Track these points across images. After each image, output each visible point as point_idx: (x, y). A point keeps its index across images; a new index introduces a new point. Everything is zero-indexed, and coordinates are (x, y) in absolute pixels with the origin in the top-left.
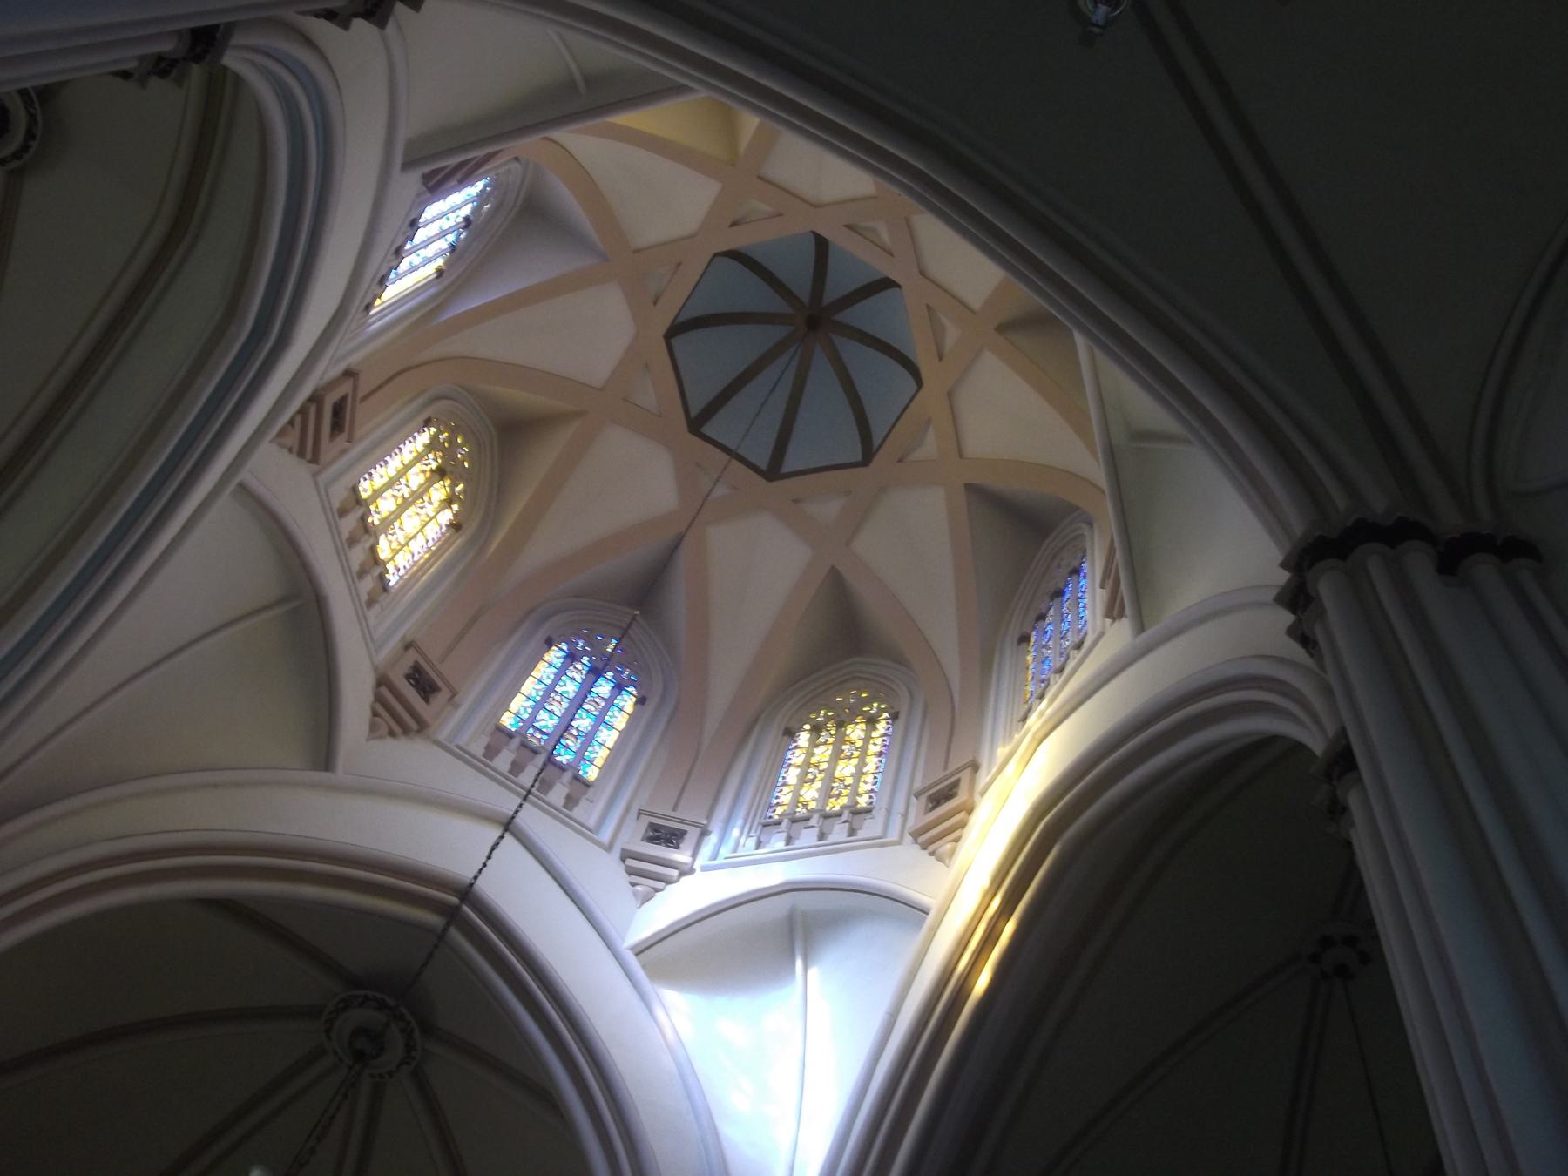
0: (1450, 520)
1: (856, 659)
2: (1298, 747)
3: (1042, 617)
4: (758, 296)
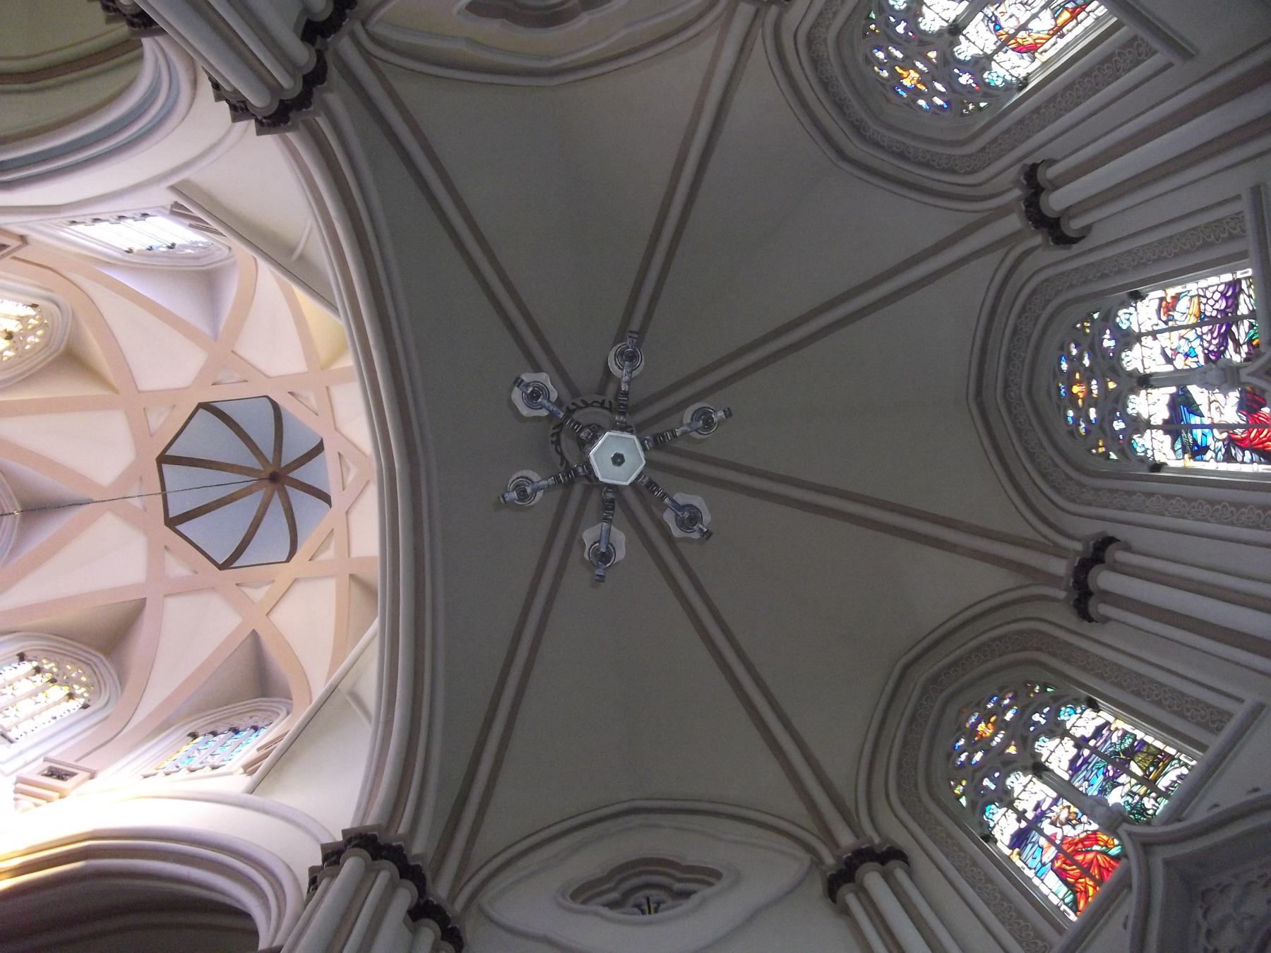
0: (440, 891)
1: (101, 656)
2: (254, 933)
3: (214, 734)
4: (264, 436)
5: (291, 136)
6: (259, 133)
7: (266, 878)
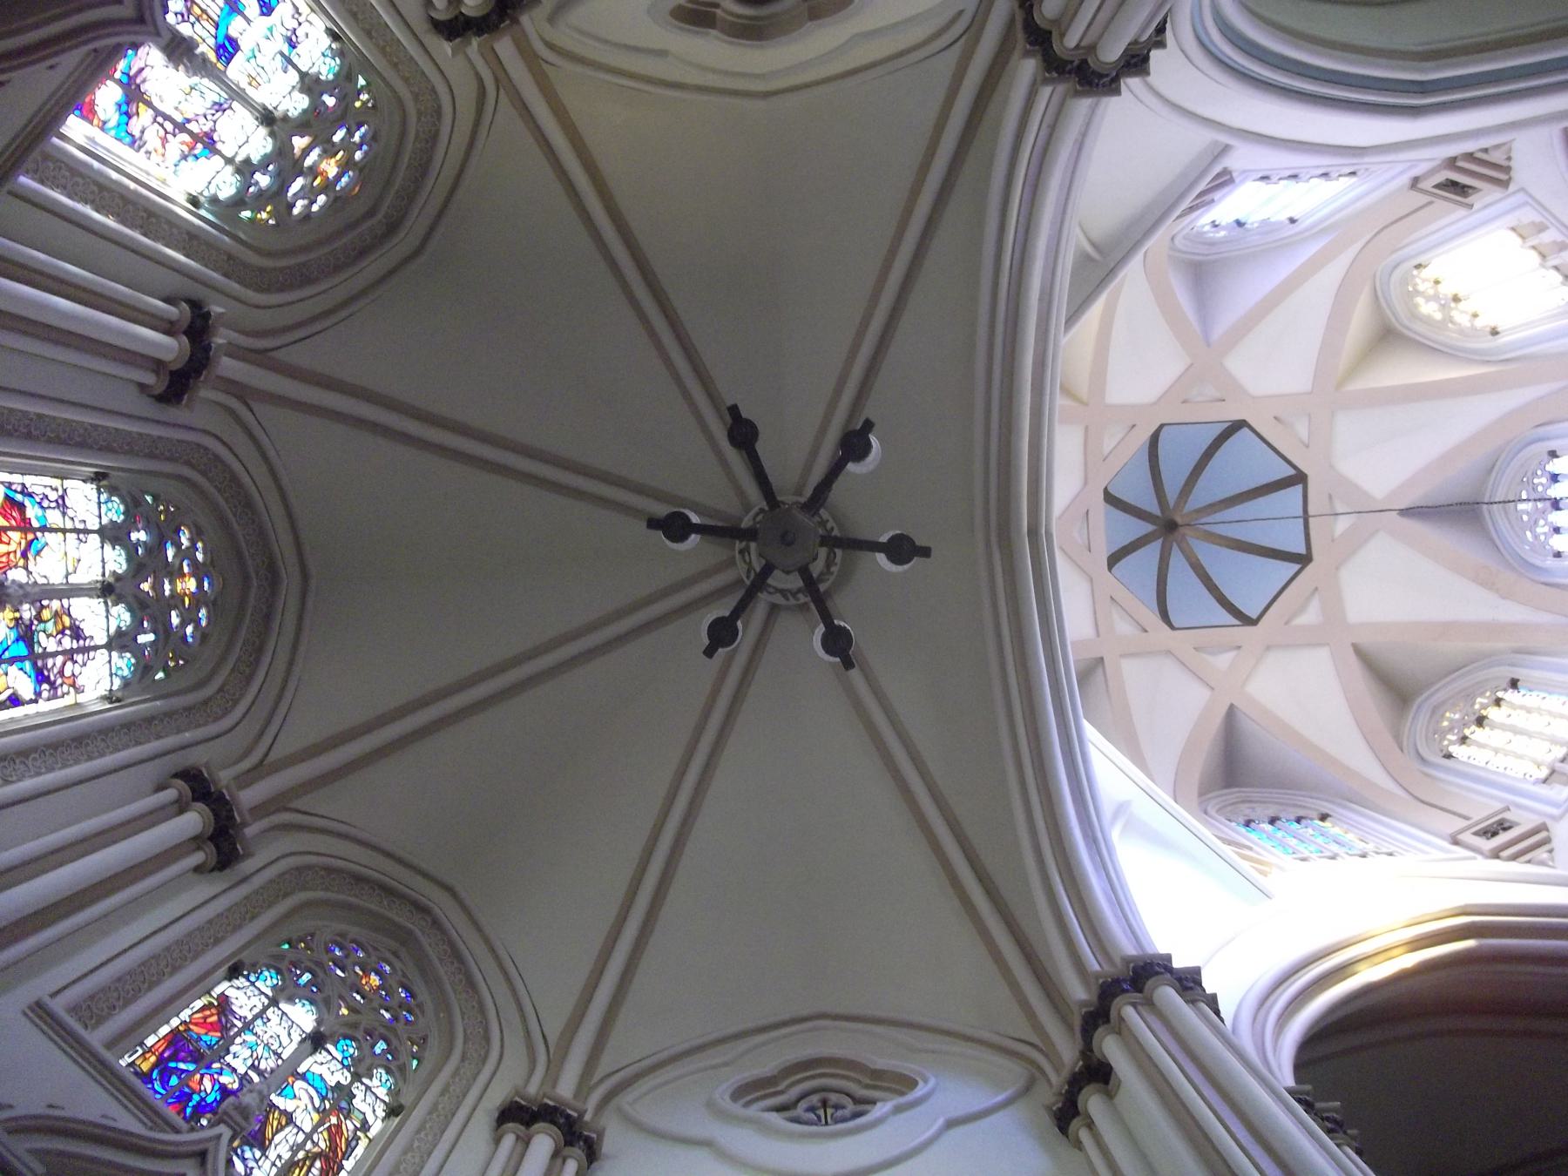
4: (1181, 577)
5: (1130, 950)
6: (1168, 958)
7: (1212, 41)
